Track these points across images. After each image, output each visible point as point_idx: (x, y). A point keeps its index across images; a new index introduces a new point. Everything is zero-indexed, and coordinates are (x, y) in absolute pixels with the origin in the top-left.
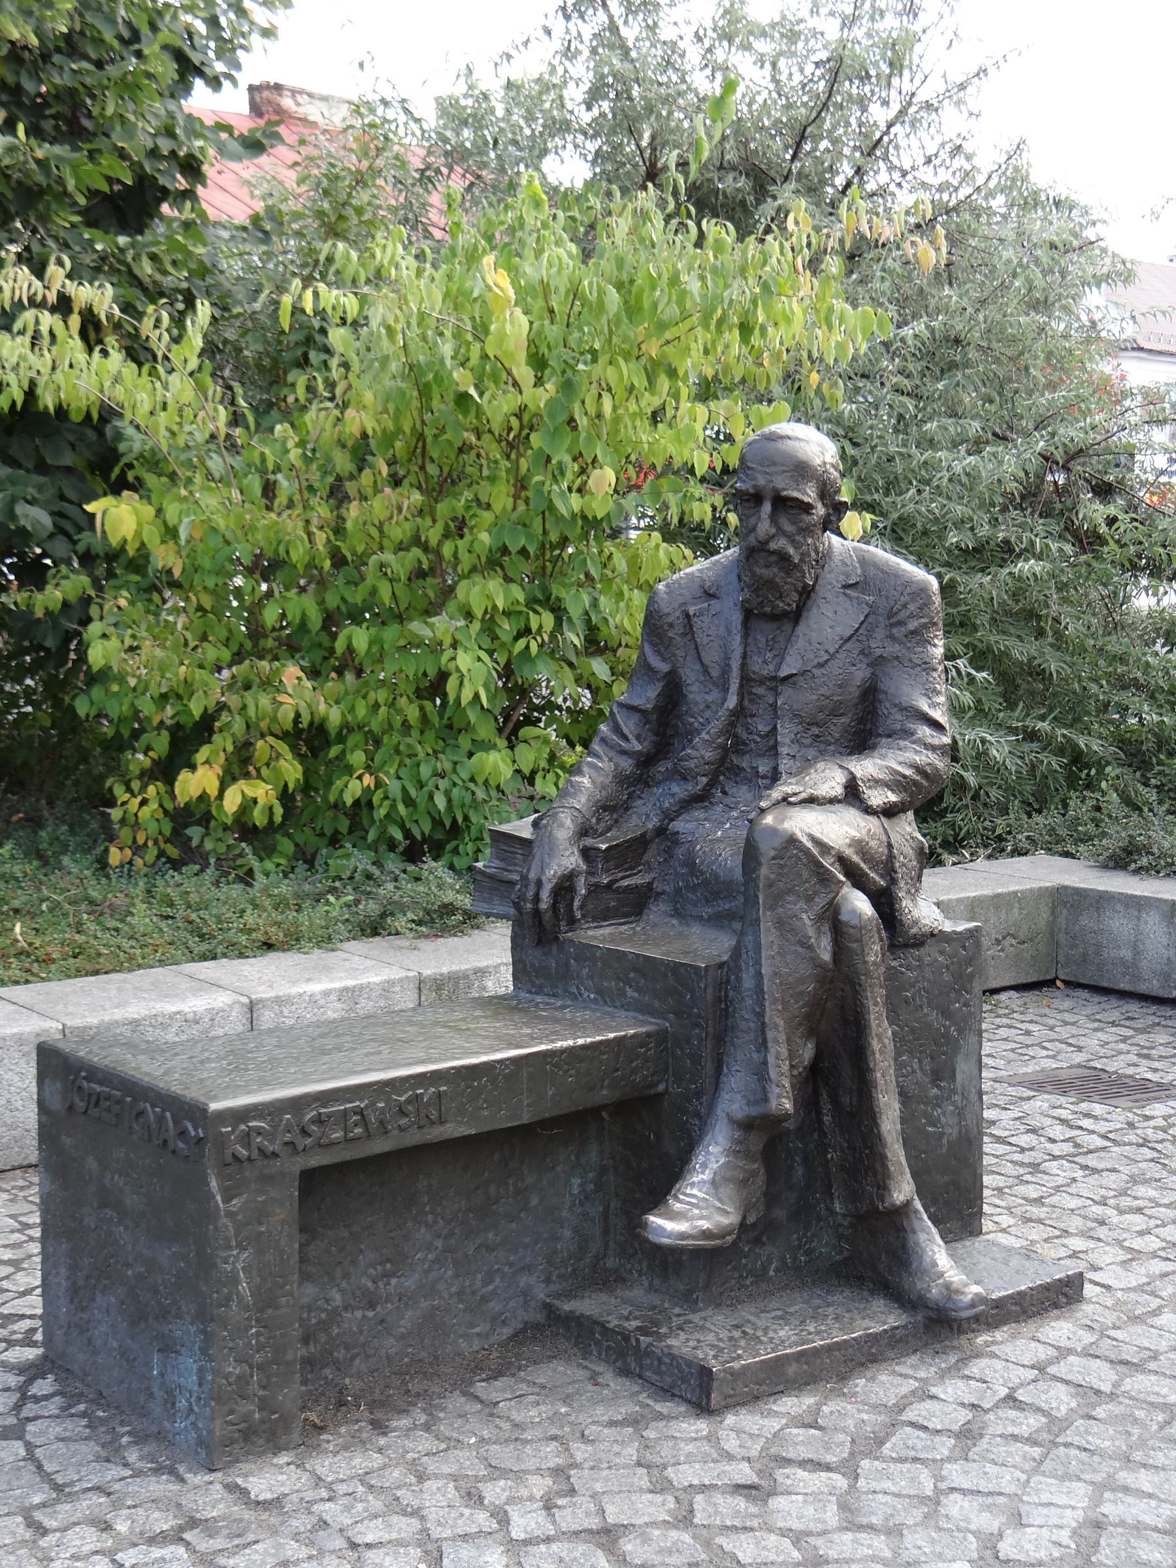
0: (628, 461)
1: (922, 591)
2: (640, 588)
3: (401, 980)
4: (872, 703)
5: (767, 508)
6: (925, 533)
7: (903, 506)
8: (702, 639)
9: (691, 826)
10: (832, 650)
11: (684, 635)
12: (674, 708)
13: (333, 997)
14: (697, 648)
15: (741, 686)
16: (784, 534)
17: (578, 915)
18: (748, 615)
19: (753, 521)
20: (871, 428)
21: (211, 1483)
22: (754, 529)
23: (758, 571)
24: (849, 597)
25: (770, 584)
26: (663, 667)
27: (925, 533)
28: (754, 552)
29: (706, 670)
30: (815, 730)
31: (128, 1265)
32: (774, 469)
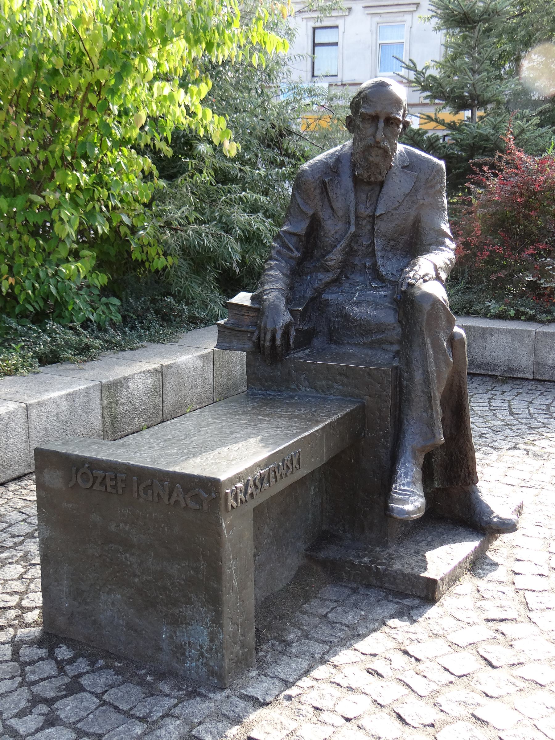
3: (93, 386)
5: (381, 125)
13: (64, 399)
17: (292, 347)
21: (228, 697)
24: (405, 172)
26: (312, 212)
30: (392, 243)
31: (135, 575)
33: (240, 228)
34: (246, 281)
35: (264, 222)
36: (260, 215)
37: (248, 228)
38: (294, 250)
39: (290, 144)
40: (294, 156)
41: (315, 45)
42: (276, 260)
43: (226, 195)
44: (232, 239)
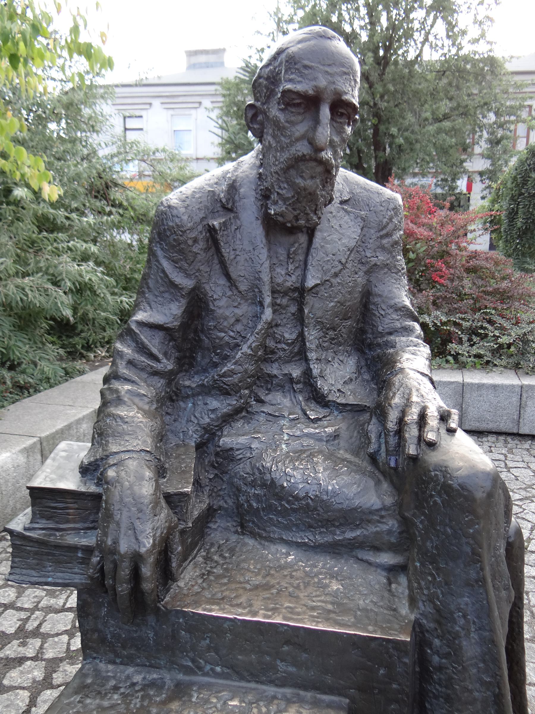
5: (325, 112)
9: (243, 440)
24: (346, 211)
26: (187, 283)
32: (335, 69)
33: (70, 280)
34: (80, 327)
35: (96, 271)
36: (91, 264)
37: (79, 279)
38: (160, 356)
39: (116, 194)
40: (120, 205)
41: (126, 129)
42: (127, 380)
43: (52, 244)
44: (61, 293)
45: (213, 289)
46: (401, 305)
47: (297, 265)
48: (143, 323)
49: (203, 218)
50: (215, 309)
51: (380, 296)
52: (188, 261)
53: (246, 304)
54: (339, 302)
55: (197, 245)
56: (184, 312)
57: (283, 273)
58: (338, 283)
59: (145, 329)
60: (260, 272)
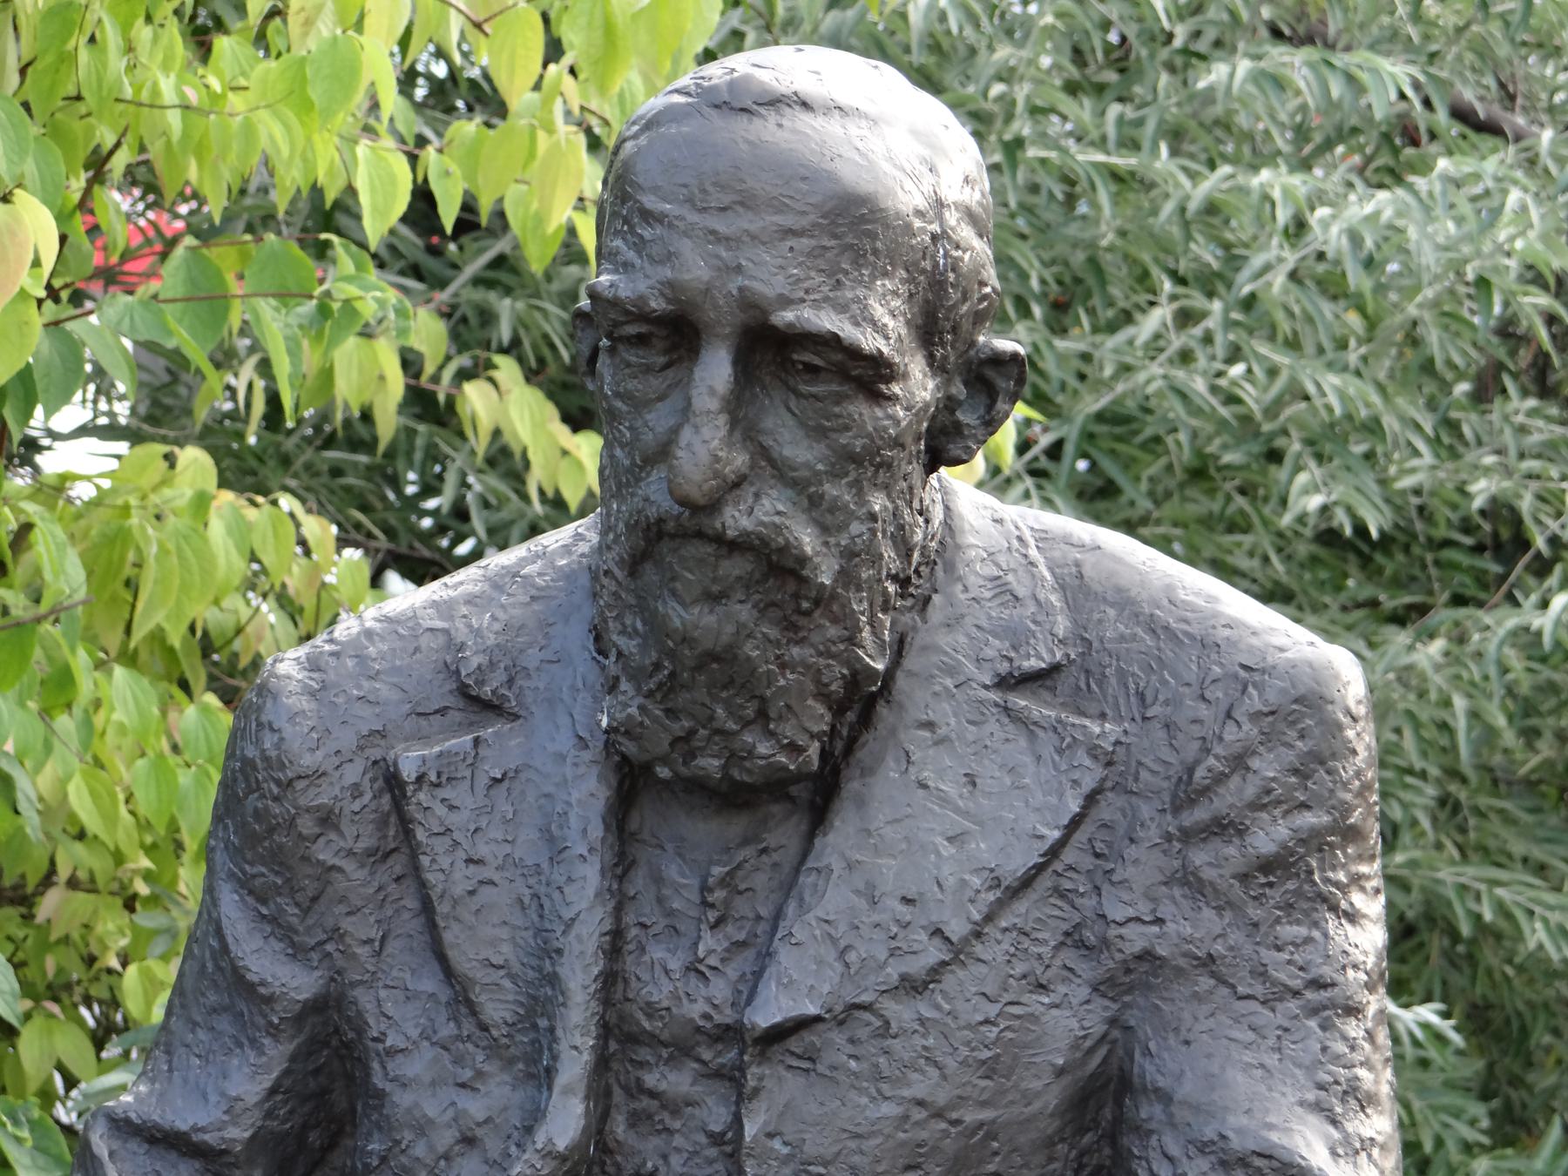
0: (97, 164)
1: (1303, 707)
2: (129, 659)
4: (1112, 1137)
5: (716, 370)
6: (1200, 473)
7: (1125, 369)
8: (446, 871)
10: (957, 929)
11: (378, 856)
12: (331, 1145)
14: (427, 908)
15: (602, 1063)
16: (782, 472)
18: (631, 782)
19: (658, 419)
20: (1007, 75)
22: (663, 453)
23: (677, 615)
25: (722, 666)
26: (295, 982)
27: (1200, 473)
28: (657, 540)
29: (462, 999)
45: (389, 1008)
46: (1252, 1145)
47: (741, 936)
48: (128, 1121)
49: (372, 733)
50: (388, 1087)
51: (1165, 1098)
52: (299, 897)
53: (506, 1078)
54: (920, 1103)
55: (333, 836)
56: (273, 1091)
57: (675, 964)
58: (922, 1021)
59: (133, 1145)
60: (559, 952)
